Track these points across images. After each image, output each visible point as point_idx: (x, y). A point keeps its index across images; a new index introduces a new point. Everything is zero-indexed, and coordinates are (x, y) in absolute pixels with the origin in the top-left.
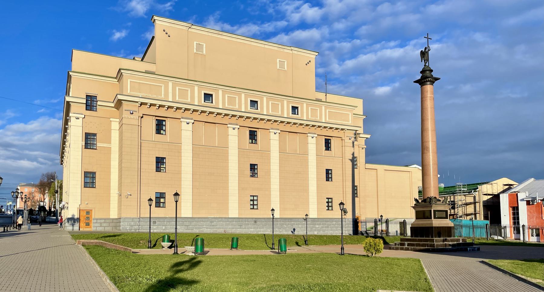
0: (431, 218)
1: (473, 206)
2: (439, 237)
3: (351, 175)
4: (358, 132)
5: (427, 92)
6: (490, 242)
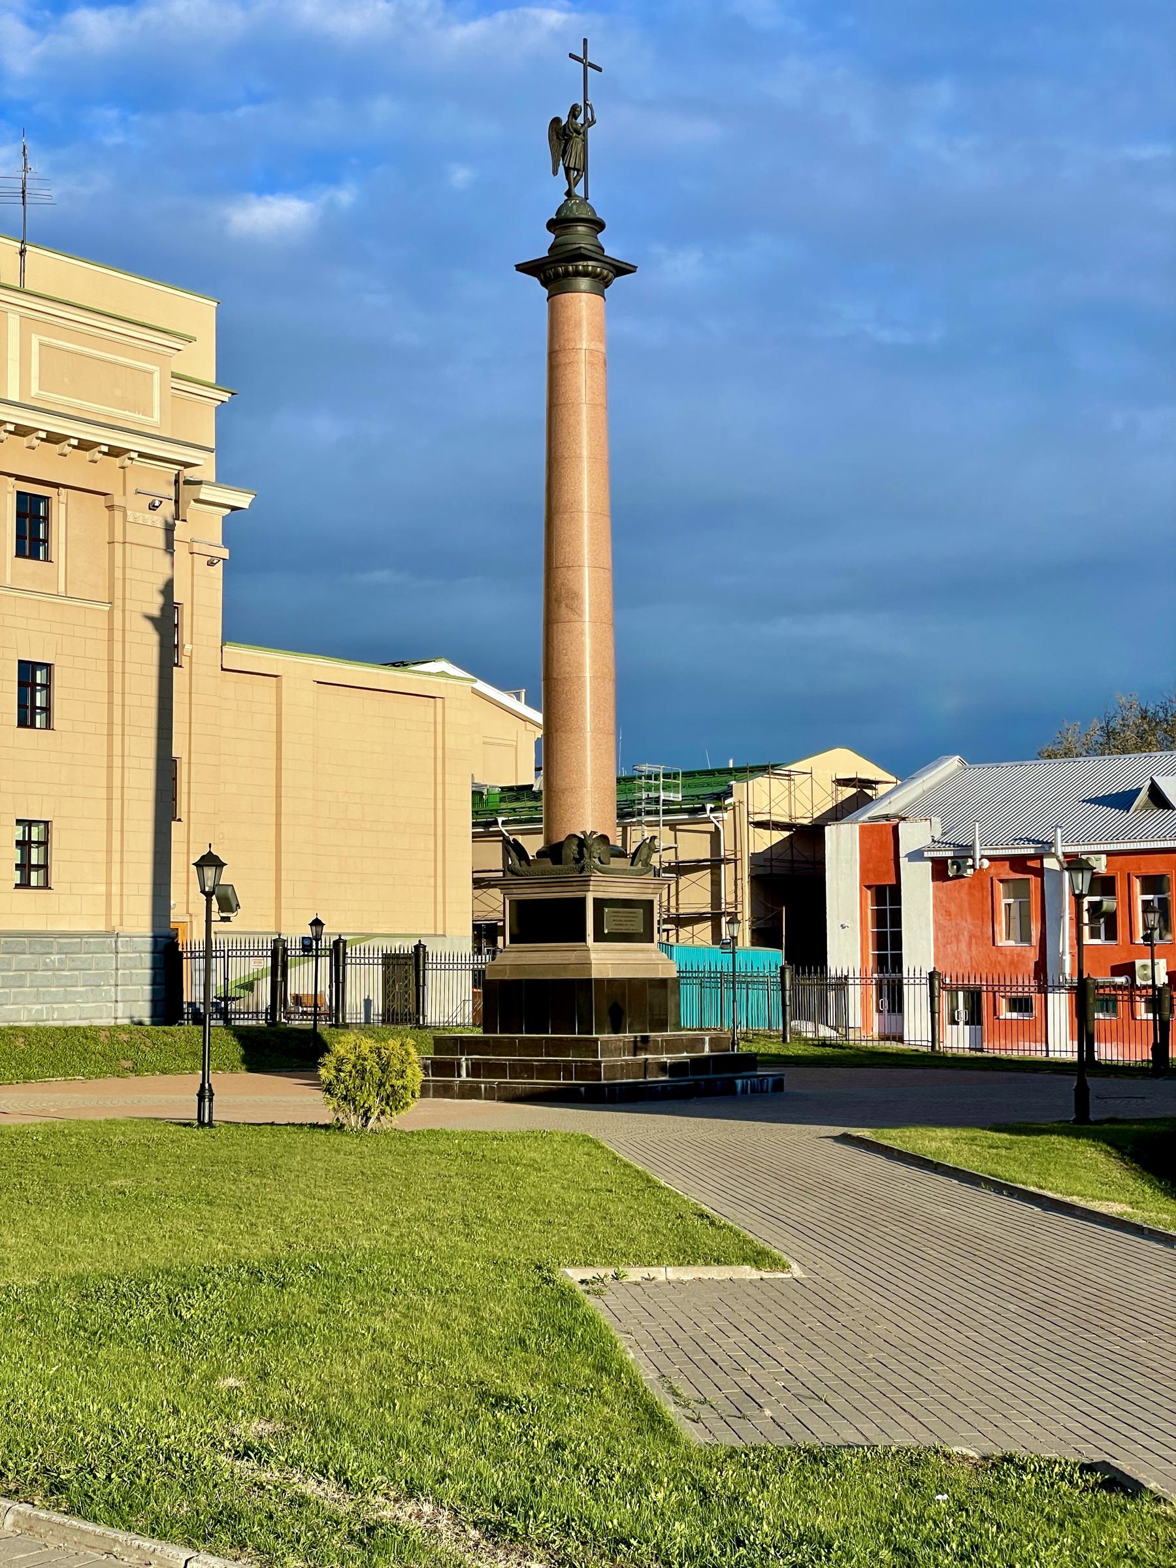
0: (583, 939)
1: (705, 877)
2: (616, 1030)
3: (152, 702)
4: (188, 473)
5: (578, 325)
6: (795, 1049)
